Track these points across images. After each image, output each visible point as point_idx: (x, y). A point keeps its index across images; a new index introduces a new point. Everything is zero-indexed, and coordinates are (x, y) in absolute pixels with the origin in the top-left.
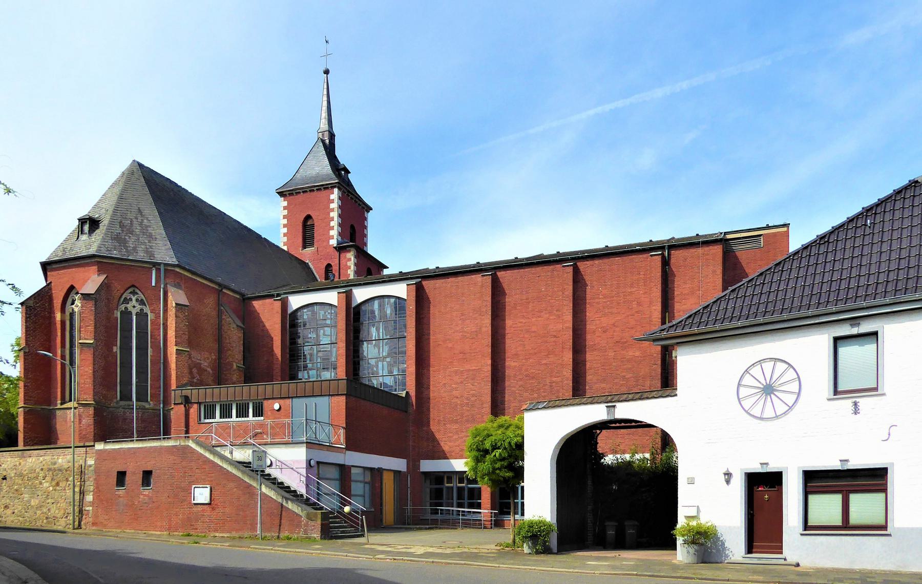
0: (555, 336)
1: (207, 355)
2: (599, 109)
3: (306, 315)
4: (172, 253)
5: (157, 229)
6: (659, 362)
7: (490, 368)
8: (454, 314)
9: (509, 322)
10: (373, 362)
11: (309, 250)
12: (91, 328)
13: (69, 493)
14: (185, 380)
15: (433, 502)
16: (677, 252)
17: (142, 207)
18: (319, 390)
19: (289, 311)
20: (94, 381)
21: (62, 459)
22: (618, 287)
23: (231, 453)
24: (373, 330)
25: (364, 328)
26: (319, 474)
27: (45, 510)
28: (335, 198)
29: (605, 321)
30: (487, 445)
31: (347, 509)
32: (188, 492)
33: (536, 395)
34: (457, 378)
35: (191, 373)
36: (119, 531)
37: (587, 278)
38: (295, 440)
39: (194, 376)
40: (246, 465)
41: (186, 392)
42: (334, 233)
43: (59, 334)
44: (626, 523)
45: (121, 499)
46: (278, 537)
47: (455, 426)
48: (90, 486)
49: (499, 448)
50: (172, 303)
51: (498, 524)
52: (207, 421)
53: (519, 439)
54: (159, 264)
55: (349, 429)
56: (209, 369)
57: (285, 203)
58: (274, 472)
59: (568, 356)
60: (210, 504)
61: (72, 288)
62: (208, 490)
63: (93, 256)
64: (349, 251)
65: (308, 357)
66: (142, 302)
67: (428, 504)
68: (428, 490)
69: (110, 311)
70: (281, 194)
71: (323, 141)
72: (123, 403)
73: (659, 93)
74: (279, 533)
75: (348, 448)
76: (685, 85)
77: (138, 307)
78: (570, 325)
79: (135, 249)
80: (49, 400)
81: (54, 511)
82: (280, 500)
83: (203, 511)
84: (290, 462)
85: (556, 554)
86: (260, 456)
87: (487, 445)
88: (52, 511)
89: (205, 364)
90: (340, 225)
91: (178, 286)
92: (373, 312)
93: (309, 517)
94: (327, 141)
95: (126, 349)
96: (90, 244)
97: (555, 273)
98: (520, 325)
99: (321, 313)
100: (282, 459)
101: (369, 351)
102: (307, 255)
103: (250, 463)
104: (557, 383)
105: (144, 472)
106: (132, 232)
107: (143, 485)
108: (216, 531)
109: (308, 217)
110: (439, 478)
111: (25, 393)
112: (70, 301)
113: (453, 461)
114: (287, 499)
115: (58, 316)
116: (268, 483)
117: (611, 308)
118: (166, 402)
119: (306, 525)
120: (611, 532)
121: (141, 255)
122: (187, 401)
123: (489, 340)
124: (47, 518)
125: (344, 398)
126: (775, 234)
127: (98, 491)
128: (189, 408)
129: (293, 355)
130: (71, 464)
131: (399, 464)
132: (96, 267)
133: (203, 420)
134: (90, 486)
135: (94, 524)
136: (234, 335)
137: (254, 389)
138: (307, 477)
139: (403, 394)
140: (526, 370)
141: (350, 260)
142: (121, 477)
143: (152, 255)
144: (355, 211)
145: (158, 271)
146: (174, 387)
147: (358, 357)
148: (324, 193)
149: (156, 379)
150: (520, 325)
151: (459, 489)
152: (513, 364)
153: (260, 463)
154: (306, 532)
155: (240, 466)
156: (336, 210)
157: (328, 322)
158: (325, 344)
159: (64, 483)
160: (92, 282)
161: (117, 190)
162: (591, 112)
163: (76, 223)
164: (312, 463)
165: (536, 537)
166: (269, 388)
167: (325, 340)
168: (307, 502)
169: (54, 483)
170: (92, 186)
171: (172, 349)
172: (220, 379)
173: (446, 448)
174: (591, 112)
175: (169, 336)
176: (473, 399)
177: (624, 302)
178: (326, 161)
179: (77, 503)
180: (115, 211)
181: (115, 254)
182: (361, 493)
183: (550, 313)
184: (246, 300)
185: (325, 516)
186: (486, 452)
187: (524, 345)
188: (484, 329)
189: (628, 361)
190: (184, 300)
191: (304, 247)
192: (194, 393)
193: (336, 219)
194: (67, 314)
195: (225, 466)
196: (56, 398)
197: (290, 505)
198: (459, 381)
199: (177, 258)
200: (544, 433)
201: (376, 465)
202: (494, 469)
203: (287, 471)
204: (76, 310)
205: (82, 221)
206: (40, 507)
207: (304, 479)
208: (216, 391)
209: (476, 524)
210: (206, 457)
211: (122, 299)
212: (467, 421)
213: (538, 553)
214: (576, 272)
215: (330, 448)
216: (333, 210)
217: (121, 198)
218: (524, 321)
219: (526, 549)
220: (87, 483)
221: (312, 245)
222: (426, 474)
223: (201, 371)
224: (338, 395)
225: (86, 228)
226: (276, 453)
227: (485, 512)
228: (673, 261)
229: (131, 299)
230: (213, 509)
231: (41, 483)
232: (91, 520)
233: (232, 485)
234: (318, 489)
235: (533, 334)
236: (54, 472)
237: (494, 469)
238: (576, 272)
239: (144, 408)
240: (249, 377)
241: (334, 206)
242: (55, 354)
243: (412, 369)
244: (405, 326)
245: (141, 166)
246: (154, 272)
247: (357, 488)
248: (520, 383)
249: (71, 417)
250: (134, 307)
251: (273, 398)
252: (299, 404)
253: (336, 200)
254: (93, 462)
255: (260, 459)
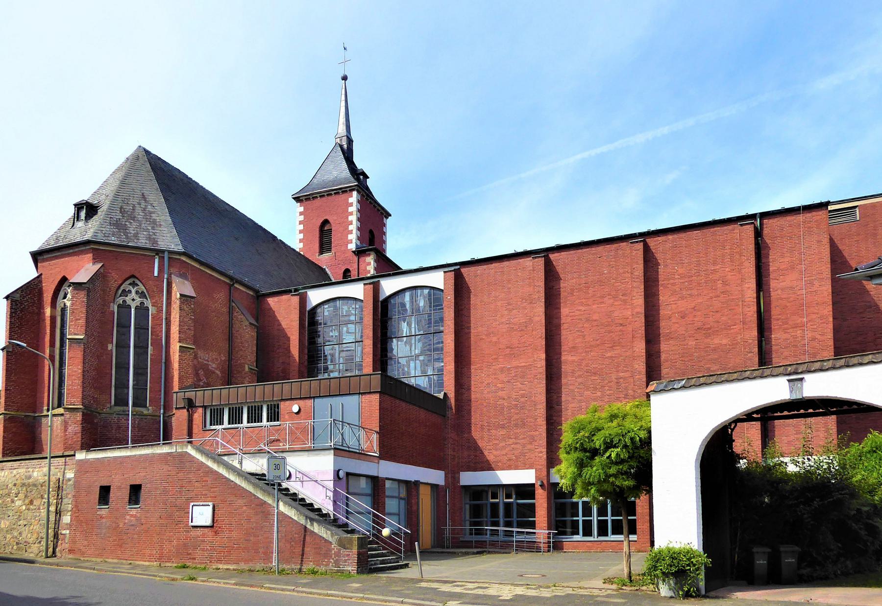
0: (621, 325)
1: (214, 355)
2: (586, 154)
3: (326, 312)
4: (177, 240)
5: (162, 215)
6: (756, 350)
7: (544, 363)
8: (499, 303)
9: (565, 311)
10: (403, 361)
11: (326, 256)
12: (82, 322)
13: (44, 513)
14: (190, 382)
15: (481, 521)
16: (771, 221)
17: (146, 193)
18: (344, 388)
19: (308, 308)
20: (83, 383)
21: (36, 471)
22: (698, 265)
23: (241, 463)
24: (404, 326)
25: (393, 324)
26: (348, 489)
27: (16, 534)
28: (351, 207)
29: (683, 305)
30: (598, 442)
31: (386, 532)
32: (185, 511)
33: (599, 394)
34: (503, 377)
35: (197, 374)
36: (99, 560)
37: (659, 256)
38: (318, 445)
39: (200, 376)
40: (261, 477)
41: (190, 394)
42: (353, 236)
43: (48, 331)
44: (782, 549)
45: (104, 520)
46: (300, 570)
47: (502, 432)
48: (68, 504)
49: (615, 447)
50: (176, 294)
51: (557, 547)
52: (213, 427)
53: (643, 434)
54: (163, 251)
55: (383, 433)
56: (218, 372)
57: (302, 209)
58: (293, 486)
59: (640, 347)
60: (212, 527)
61: (64, 280)
62: (210, 508)
63: (88, 242)
64: (369, 255)
65: (329, 357)
66: (142, 295)
67: (468, 523)
68: (468, 507)
69: (106, 304)
70: (297, 199)
71: (341, 146)
72: (118, 408)
73: (640, 138)
74: (301, 564)
75: (381, 457)
76: (665, 130)
77: (138, 300)
78: (641, 309)
79: (136, 236)
80: (34, 405)
81: (27, 535)
82: (302, 521)
83: (203, 535)
84: (313, 473)
85: (705, 597)
86: (278, 464)
87: (598, 442)
88: (24, 536)
89: (213, 366)
90: (359, 229)
91: (183, 276)
92: (403, 305)
93: (342, 544)
94: (345, 147)
95: (123, 346)
96: (86, 230)
97: (620, 252)
98: (578, 313)
99: (344, 308)
100: (304, 469)
101: (399, 348)
102: (324, 260)
103: (264, 475)
104: (624, 378)
105: (131, 486)
106: (134, 218)
107: (100, 503)
108: (219, 561)
109: (326, 222)
110: (477, 492)
111: (6, 398)
112: (61, 294)
113: (500, 473)
114: (312, 520)
115: (48, 311)
116: (287, 499)
117: (691, 289)
118: (167, 407)
119: (338, 554)
120: (761, 562)
121: (143, 242)
122: (190, 405)
123: (542, 331)
124: (17, 544)
125: (377, 396)
126: (873, 205)
127: (77, 509)
128: (193, 412)
129: (313, 359)
130: (47, 478)
131: (436, 477)
132: (90, 255)
133: (208, 427)
134: (68, 504)
135: (71, 551)
136: (247, 334)
137: (268, 388)
138: (335, 492)
139: (441, 396)
140: (587, 365)
141: (369, 264)
142: (105, 493)
143: (155, 242)
144: (374, 216)
145: (162, 259)
146: (176, 389)
147: (386, 356)
148: (344, 196)
149: (156, 381)
150: (578, 313)
151: (508, 506)
152: (570, 358)
153: (277, 473)
154: (337, 564)
155: (253, 479)
156: (355, 213)
157: (352, 318)
158: (348, 343)
159: (39, 500)
160: (84, 270)
161: (120, 175)
162: (579, 157)
163: (72, 211)
164: (341, 474)
165: (676, 569)
166: (286, 387)
167: (348, 338)
168: (335, 522)
169: (27, 501)
170: (94, 172)
171: (175, 346)
172: (230, 378)
173: (490, 456)
174: (579, 157)
175: (172, 332)
176: (522, 400)
177: (706, 282)
178: (344, 165)
179: (52, 525)
180: (117, 195)
181: (113, 240)
182: (395, 511)
183: (615, 297)
184: (260, 297)
185: (363, 542)
186: (595, 452)
187: (584, 336)
188: (536, 319)
189: (714, 350)
190: (189, 291)
191: (321, 253)
192: (198, 396)
193: (355, 222)
194: (59, 309)
195: (232, 477)
196: (43, 403)
197: (316, 528)
198: (506, 380)
199: (184, 247)
200: (680, 425)
201: (412, 478)
202: (608, 476)
203: (309, 485)
204: (68, 304)
205: (79, 207)
206: (10, 530)
207: (331, 494)
208: (225, 392)
209: (532, 547)
210: (208, 467)
211: (120, 291)
212: (516, 425)
213: (687, 595)
214: (647, 249)
215: (361, 455)
216: (351, 214)
217: (123, 183)
218: (583, 309)
219: (664, 590)
220: (65, 501)
221: (329, 250)
222: (466, 488)
223: (209, 373)
224: (370, 393)
225: (83, 214)
226: (296, 462)
227: (541, 533)
228: (766, 231)
229: (130, 292)
230: (216, 533)
231: (13, 501)
232: (67, 546)
233: (241, 502)
234: (347, 505)
235: (595, 323)
236: (28, 486)
237: (608, 476)
238: (647, 249)
239: (142, 415)
240: (265, 372)
241: (353, 209)
242: (44, 352)
243: (449, 366)
244: (442, 320)
245: (147, 152)
246: (157, 261)
247: (391, 505)
248: (580, 380)
249: (57, 425)
250: (133, 300)
251: (291, 399)
252: (323, 404)
253: (355, 204)
254: (72, 475)
255: (277, 467)
